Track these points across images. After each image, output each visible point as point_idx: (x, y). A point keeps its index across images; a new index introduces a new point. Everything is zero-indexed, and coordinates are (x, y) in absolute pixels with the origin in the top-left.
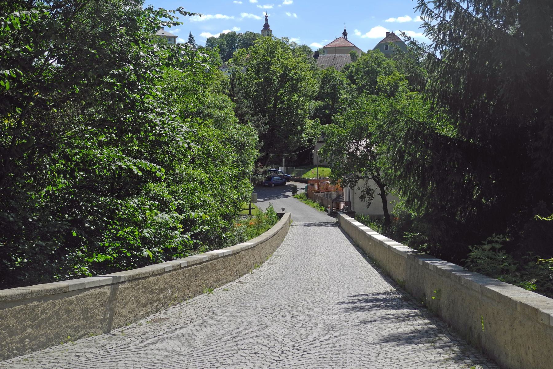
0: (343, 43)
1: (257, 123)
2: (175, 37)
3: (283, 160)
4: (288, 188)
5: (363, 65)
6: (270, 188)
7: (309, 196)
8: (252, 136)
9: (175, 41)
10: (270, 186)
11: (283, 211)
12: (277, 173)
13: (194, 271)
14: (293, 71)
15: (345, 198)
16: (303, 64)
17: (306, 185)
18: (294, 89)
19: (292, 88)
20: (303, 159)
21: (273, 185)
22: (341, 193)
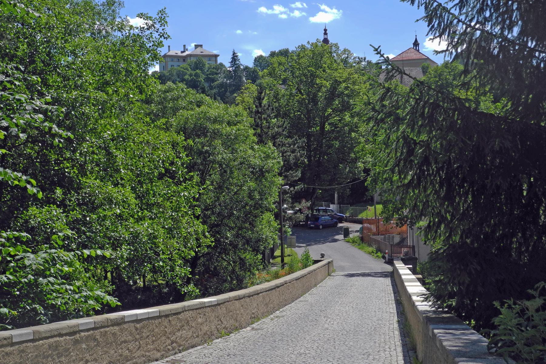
0: (414, 55)
1: (292, 147)
2: (216, 56)
3: (336, 195)
4: (338, 231)
5: (435, 77)
6: (315, 229)
7: (364, 240)
8: (274, 158)
9: (216, 61)
10: (317, 228)
11: (323, 257)
12: (326, 212)
13: (55, 347)
14: (344, 85)
15: (410, 243)
16: (356, 76)
17: (360, 226)
18: (346, 107)
19: (343, 106)
20: (358, 195)
21: (321, 227)
22: (405, 236)
